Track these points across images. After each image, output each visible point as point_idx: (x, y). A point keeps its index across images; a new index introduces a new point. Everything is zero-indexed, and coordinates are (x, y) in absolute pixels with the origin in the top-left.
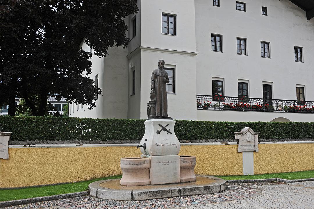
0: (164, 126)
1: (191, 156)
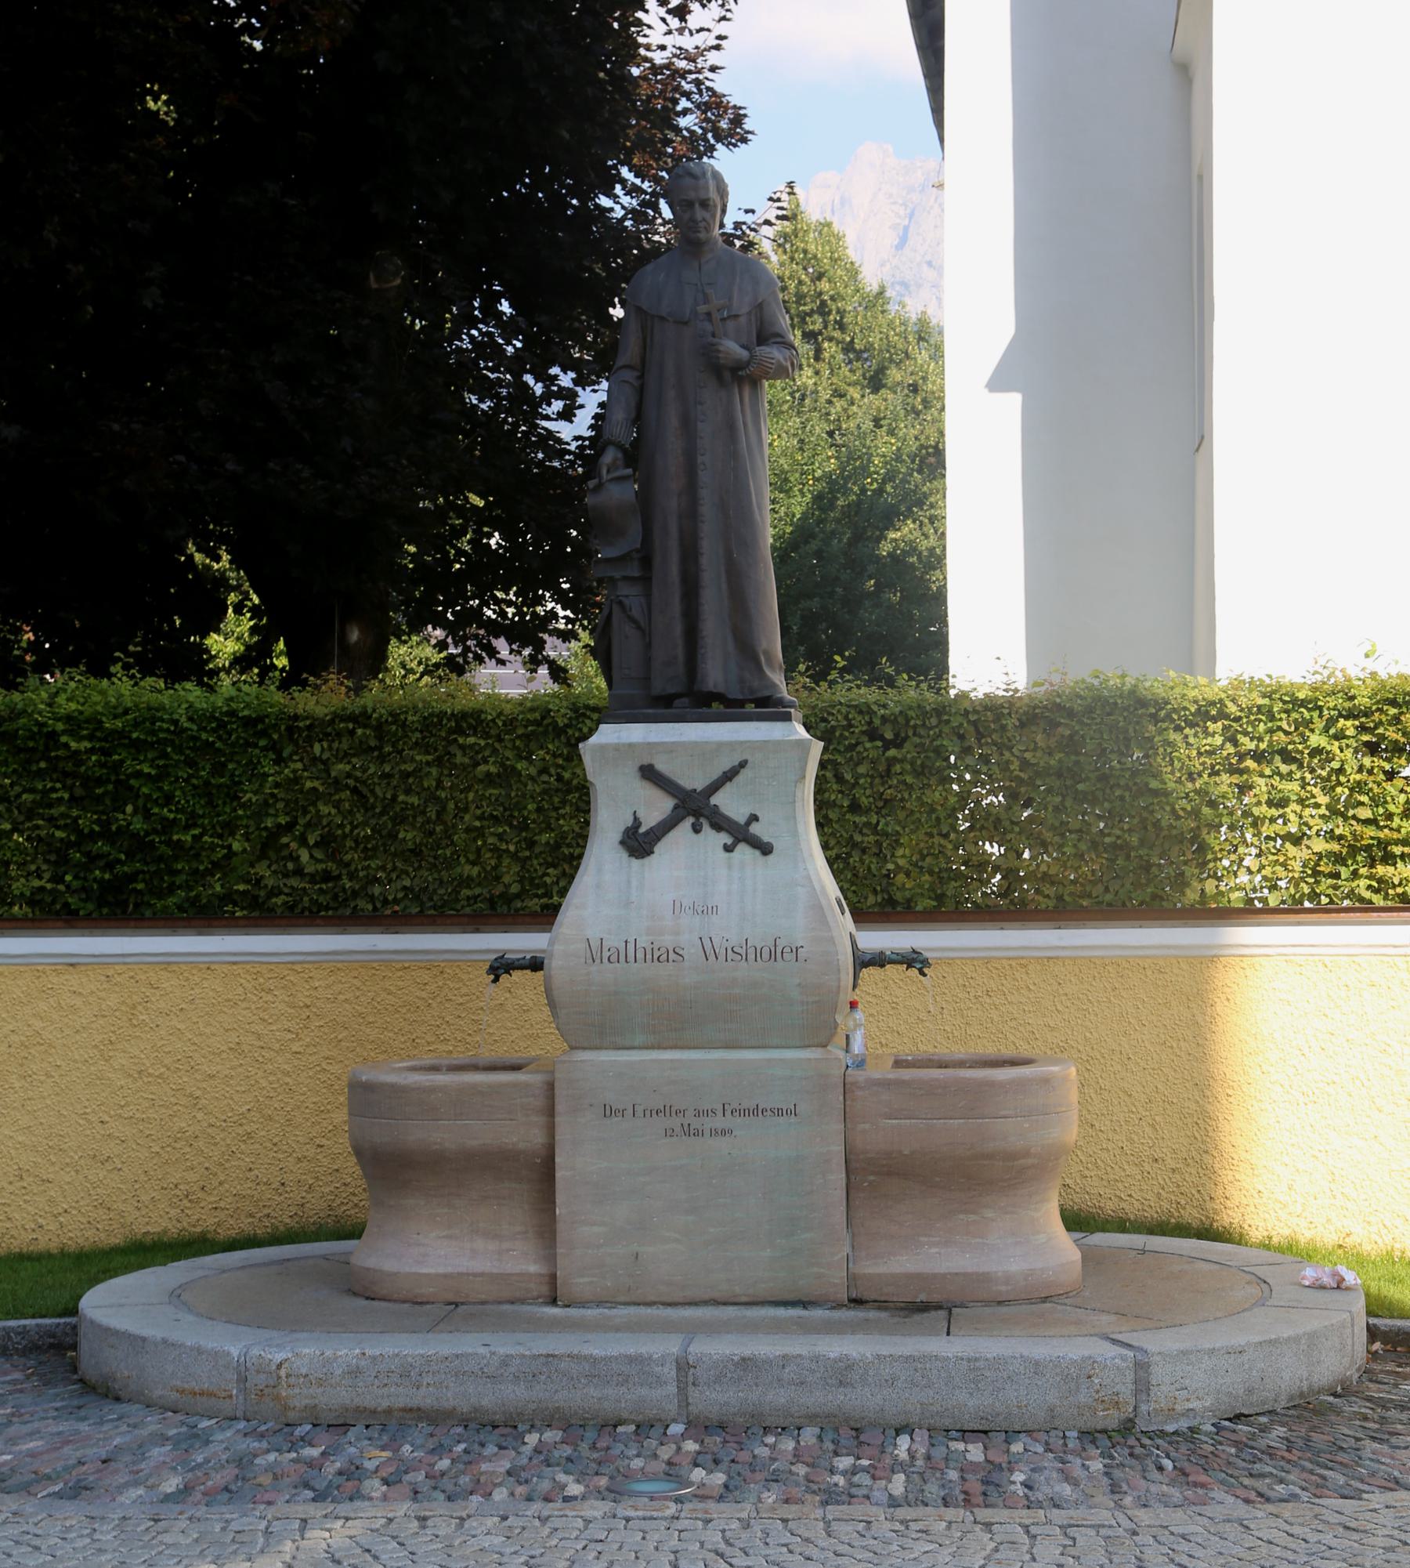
0: (694, 780)
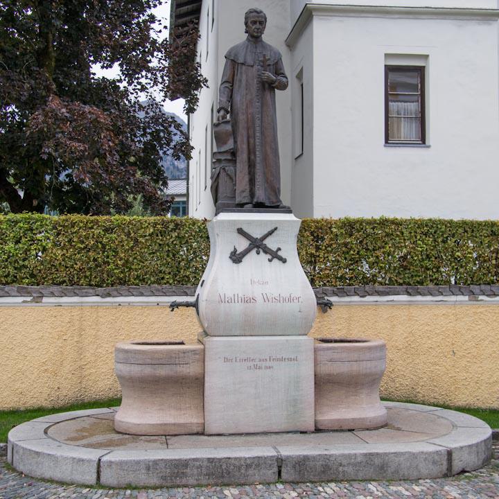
0: (257, 234)
1: (182, 343)
